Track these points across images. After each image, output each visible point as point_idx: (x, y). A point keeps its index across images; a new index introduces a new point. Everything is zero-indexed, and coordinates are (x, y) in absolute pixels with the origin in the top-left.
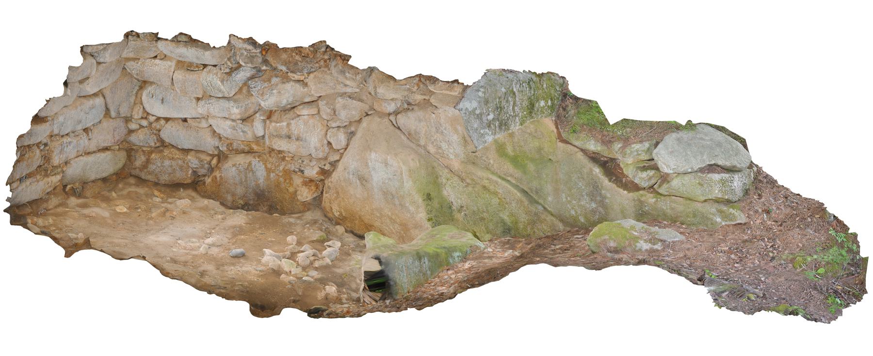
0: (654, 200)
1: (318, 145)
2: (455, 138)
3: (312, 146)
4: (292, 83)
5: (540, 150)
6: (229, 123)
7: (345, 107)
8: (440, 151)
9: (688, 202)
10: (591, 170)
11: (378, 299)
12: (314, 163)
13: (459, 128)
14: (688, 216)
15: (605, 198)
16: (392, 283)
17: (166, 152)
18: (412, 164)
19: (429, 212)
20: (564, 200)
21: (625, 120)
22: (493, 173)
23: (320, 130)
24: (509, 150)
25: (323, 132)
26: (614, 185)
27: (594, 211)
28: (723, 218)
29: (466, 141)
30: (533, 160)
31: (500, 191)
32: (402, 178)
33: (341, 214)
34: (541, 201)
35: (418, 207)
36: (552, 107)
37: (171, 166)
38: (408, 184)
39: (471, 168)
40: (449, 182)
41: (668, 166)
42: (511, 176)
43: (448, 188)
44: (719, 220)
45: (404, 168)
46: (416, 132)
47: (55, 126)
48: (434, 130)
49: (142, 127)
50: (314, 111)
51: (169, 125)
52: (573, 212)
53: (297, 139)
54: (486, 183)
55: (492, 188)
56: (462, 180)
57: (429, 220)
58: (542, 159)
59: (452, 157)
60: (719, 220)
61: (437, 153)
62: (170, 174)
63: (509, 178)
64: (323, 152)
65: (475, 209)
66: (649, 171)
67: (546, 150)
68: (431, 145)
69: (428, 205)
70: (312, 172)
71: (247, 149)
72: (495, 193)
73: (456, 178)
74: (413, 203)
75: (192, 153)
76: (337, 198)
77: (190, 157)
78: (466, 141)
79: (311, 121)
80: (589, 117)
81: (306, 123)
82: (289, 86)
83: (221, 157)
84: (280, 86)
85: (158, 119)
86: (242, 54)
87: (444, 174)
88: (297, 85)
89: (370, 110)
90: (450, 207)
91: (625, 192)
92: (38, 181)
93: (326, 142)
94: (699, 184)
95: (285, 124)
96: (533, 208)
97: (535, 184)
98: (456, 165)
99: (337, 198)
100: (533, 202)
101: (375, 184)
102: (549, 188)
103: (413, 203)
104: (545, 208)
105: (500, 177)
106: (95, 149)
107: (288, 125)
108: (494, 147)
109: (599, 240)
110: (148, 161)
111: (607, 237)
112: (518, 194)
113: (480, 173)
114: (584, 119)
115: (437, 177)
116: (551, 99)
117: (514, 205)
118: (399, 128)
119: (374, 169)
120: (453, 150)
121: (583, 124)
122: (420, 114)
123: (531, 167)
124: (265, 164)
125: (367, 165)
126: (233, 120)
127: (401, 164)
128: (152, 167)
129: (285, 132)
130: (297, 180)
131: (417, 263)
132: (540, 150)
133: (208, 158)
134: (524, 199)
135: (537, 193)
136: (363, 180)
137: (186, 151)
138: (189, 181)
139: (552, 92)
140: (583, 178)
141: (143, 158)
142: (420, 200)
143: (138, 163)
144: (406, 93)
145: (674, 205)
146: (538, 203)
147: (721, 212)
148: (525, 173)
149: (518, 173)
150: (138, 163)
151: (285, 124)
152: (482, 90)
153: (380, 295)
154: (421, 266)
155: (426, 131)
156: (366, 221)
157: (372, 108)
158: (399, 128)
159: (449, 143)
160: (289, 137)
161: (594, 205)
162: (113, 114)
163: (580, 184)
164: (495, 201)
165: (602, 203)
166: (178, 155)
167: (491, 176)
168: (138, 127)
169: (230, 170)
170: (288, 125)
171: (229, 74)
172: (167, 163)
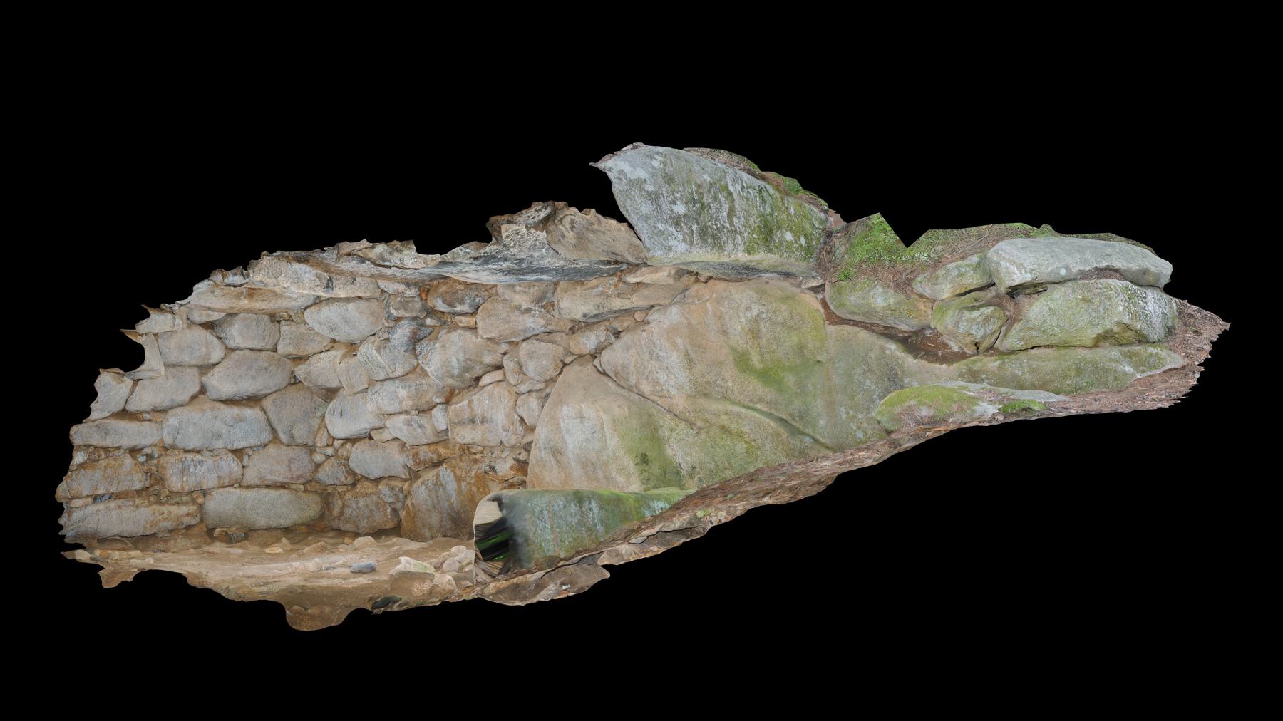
0: (997, 364)
2: (675, 358)
4: (459, 331)
5: (801, 348)
6: (403, 417)
7: (531, 355)
8: (658, 388)
9: (1063, 351)
10: (883, 349)
11: (496, 572)
12: (506, 453)
13: (679, 340)
14: (1065, 377)
16: (520, 540)
18: (617, 412)
20: (844, 416)
22: (734, 403)
23: (507, 401)
24: (756, 361)
25: (512, 403)
26: (924, 362)
28: (1136, 367)
29: (690, 360)
31: (746, 430)
32: (604, 435)
34: (809, 431)
35: (629, 475)
36: (808, 248)
37: (367, 506)
38: (613, 442)
39: (702, 402)
40: (674, 435)
41: (1020, 266)
42: (761, 400)
43: (673, 444)
44: (1129, 369)
45: (605, 417)
47: (165, 432)
48: (647, 356)
49: (328, 457)
50: (497, 375)
52: (860, 435)
53: (482, 422)
54: (724, 420)
56: (691, 425)
58: (805, 362)
59: (674, 391)
60: (1129, 369)
61: (653, 393)
62: (368, 518)
63: (758, 406)
64: (515, 433)
65: (712, 466)
66: (983, 309)
67: (810, 346)
68: (645, 382)
69: (642, 471)
70: (505, 467)
72: (740, 435)
73: (683, 425)
74: (622, 470)
75: (384, 482)
77: (382, 487)
78: (690, 360)
80: (868, 246)
81: (490, 396)
82: (455, 335)
85: (347, 440)
87: (666, 421)
88: (468, 333)
89: (566, 355)
90: (678, 473)
91: (944, 366)
92: (137, 507)
93: (516, 418)
94: (1084, 300)
95: (465, 402)
96: (796, 443)
97: (797, 405)
98: (680, 403)
100: (795, 432)
101: (570, 455)
102: (819, 405)
103: (622, 470)
104: (815, 440)
105: (744, 406)
106: (257, 482)
107: (470, 402)
108: (731, 357)
109: (898, 410)
111: (913, 402)
112: (772, 424)
113: (715, 406)
115: (656, 429)
116: (806, 237)
117: (767, 447)
118: (605, 374)
119: (568, 431)
120: (673, 379)
121: (862, 262)
124: (453, 471)
126: (407, 412)
127: (601, 413)
129: (466, 416)
131: (573, 508)
132: (801, 348)
133: (400, 485)
134: (782, 430)
135: (801, 418)
136: (557, 452)
137: (377, 481)
139: (807, 226)
140: (871, 370)
142: (632, 464)
144: (599, 300)
145: (1035, 364)
146: (803, 434)
147: (1130, 356)
148: (781, 391)
149: (769, 393)
151: (465, 402)
152: (660, 159)
153: (499, 565)
154: (583, 515)
155: (636, 362)
157: (568, 352)
158: (605, 374)
159: (668, 371)
160: (473, 421)
162: (283, 437)
163: (868, 383)
164: (740, 447)
166: (369, 487)
167: (731, 408)
168: (323, 458)
170: (470, 402)
172: (362, 502)
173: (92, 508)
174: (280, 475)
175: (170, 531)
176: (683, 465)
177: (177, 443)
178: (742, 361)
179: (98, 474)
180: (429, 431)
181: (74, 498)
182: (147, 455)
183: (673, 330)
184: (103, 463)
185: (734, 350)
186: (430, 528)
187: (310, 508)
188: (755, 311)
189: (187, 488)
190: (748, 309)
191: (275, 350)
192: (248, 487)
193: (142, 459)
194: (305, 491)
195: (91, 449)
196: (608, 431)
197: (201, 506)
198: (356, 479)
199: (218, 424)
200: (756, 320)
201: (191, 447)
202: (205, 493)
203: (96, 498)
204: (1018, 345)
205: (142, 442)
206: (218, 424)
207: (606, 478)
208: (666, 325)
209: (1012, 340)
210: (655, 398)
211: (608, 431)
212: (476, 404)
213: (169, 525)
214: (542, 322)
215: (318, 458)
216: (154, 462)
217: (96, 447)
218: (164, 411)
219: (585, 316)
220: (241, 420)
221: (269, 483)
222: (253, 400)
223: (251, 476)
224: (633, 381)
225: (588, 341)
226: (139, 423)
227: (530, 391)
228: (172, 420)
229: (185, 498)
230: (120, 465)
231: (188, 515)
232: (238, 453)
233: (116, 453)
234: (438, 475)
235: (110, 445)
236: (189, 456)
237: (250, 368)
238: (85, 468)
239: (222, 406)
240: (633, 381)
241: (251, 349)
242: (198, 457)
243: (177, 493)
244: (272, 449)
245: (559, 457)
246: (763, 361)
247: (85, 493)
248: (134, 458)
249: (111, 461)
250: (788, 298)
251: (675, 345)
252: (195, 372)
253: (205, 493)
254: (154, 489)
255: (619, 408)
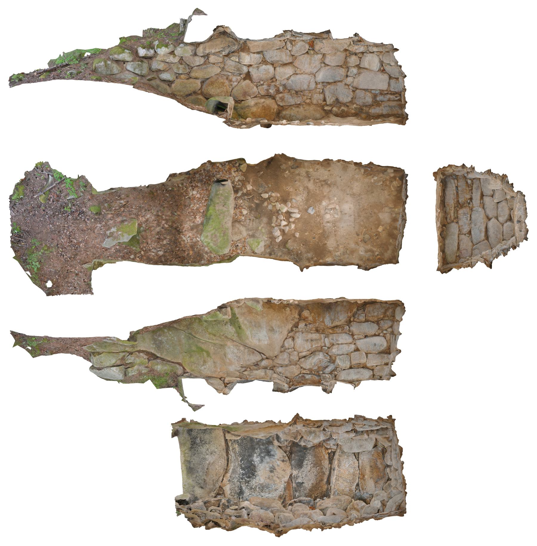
1: (297, 340)
2: (229, 356)
3: (300, 338)
5: (191, 357)
6: (340, 343)
7: (284, 360)
10: (161, 355)
12: (300, 330)
13: (228, 361)
15: (153, 344)
17: (376, 319)
19: (238, 321)
21: (143, 383)
24: (205, 354)
27: (160, 336)
30: (194, 351)
33: (285, 310)
38: (248, 333)
42: (203, 343)
45: (251, 340)
46: (250, 355)
49: (386, 330)
50: (301, 354)
51: (373, 333)
52: (170, 333)
53: (308, 340)
54: (214, 338)
55: (212, 336)
56: (226, 337)
57: (237, 318)
58: (190, 353)
59: (232, 347)
65: (219, 325)
70: (302, 325)
71: (335, 329)
72: (210, 334)
73: (229, 337)
74: (245, 325)
76: (287, 316)
78: (225, 355)
79: (301, 350)
81: (304, 348)
83: (349, 322)
84: (311, 367)
85: (379, 335)
86: (329, 379)
88: (305, 367)
96: (190, 331)
97: (191, 341)
98: (229, 343)
99: (287, 316)
102: (184, 341)
107: (312, 346)
110: (385, 313)
114: (163, 380)
119: (265, 336)
122: (248, 363)
123: (194, 348)
125: (269, 338)
128: (383, 311)
129: (314, 343)
130: (310, 318)
134: (194, 335)
136: (272, 330)
137: (367, 321)
138: (367, 306)
141: (388, 313)
142: (242, 326)
143: (391, 310)
145: (117, 349)
147: (94, 349)
148: (196, 345)
149: (200, 345)
150: (391, 310)
151: (314, 346)
156: (271, 310)
159: (233, 352)
160: (312, 340)
161: (160, 339)
165: (155, 340)
166: (371, 319)
169: (342, 318)
170: (312, 346)
171: (336, 368)
176: (229, 325)
178: (208, 354)
180: (330, 338)
183: (231, 364)
185: (210, 357)
186: (343, 305)
188: (203, 368)
190: (205, 368)
196: (250, 336)
198: (378, 323)
200: (203, 365)
202: (457, 223)
204: (121, 353)
207: (251, 322)
208: (233, 366)
209: (122, 355)
210: (240, 345)
211: (250, 336)
212: (310, 345)
215: (390, 330)
224: (246, 350)
225: (264, 363)
234: (332, 323)
240: (246, 350)
242: (469, 219)
245: (271, 329)
246: (203, 354)
250: (193, 370)
251: (229, 360)
252: (496, 215)
253: (457, 223)
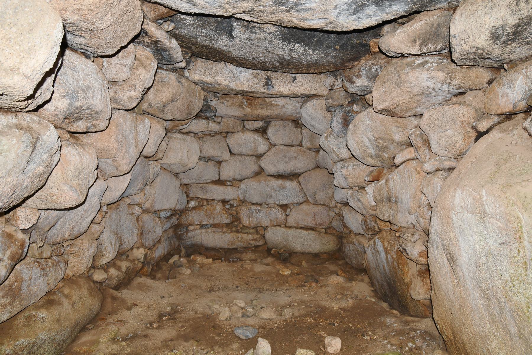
92: (224, 233)
106: (294, 225)
170: (387, 181)
173: (199, 231)
174: (309, 221)
175: (245, 248)
177: (246, 198)
179: (202, 213)
181: (190, 225)
182: (230, 205)
184: (205, 207)
187: (328, 244)
189: (252, 225)
191: (301, 145)
192: (290, 227)
193: (228, 207)
194: (326, 233)
195: (199, 200)
197: (263, 236)
199: (269, 189)
201: (255, 202)
202: (265, 228)
203: (202, 226)
205: (227, 198)
206: (269, 189)
213: (241, 244)
214: (442, 75)
216: (234, 209)
217: (201, 199)
218: (240, 181)
219: (495, 37)
220: (284, 188)
221: (303, 226)
222: (294, 176)
223: (291, 221)
226: (225, 187)
227: (438, 170)
228: (243, 186)
229: (251, 231)
230: (214, 209)
231: (253, 240)
232: (284, 207)
233: (212, 202)
235: (208, 198)
236: (253, 207)
237: (284, 156)
238: (195, 210)
239: (272, 179)
241: (285, 145)
242: (259, 208)
243: (247, 227)
244: (304, 207)
247: (196, 223)
248: (224, 206)
249: (209, 207)
253: (265, 228)
254: (234, 224)
255: (97, 305)
